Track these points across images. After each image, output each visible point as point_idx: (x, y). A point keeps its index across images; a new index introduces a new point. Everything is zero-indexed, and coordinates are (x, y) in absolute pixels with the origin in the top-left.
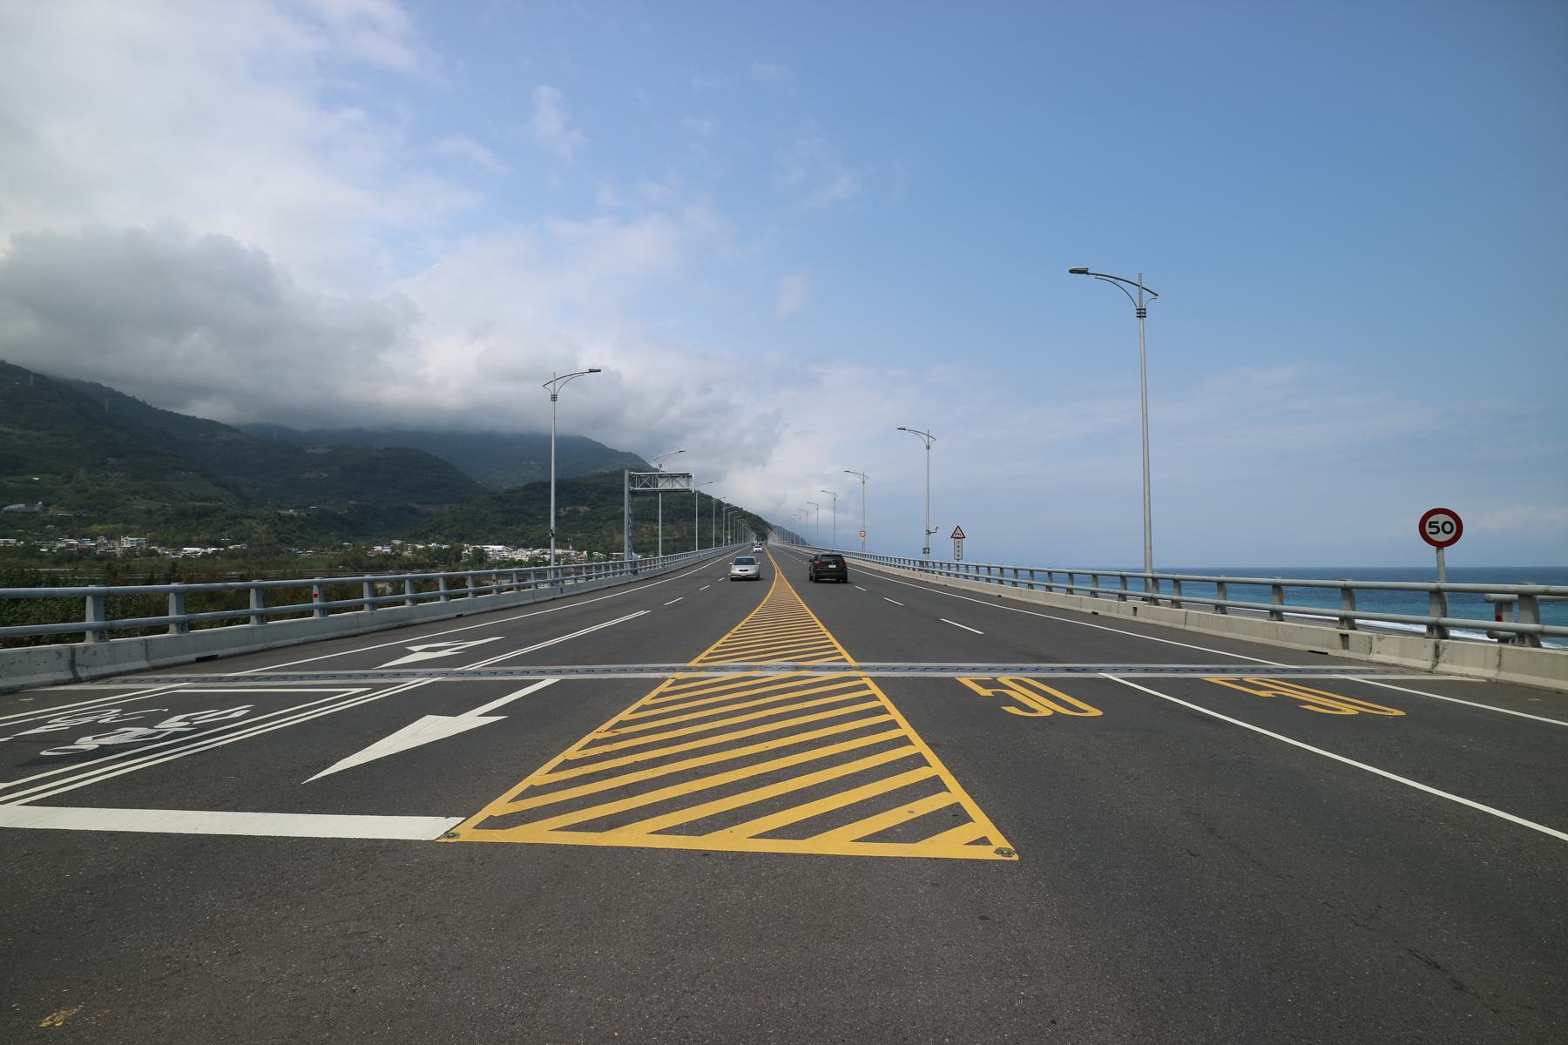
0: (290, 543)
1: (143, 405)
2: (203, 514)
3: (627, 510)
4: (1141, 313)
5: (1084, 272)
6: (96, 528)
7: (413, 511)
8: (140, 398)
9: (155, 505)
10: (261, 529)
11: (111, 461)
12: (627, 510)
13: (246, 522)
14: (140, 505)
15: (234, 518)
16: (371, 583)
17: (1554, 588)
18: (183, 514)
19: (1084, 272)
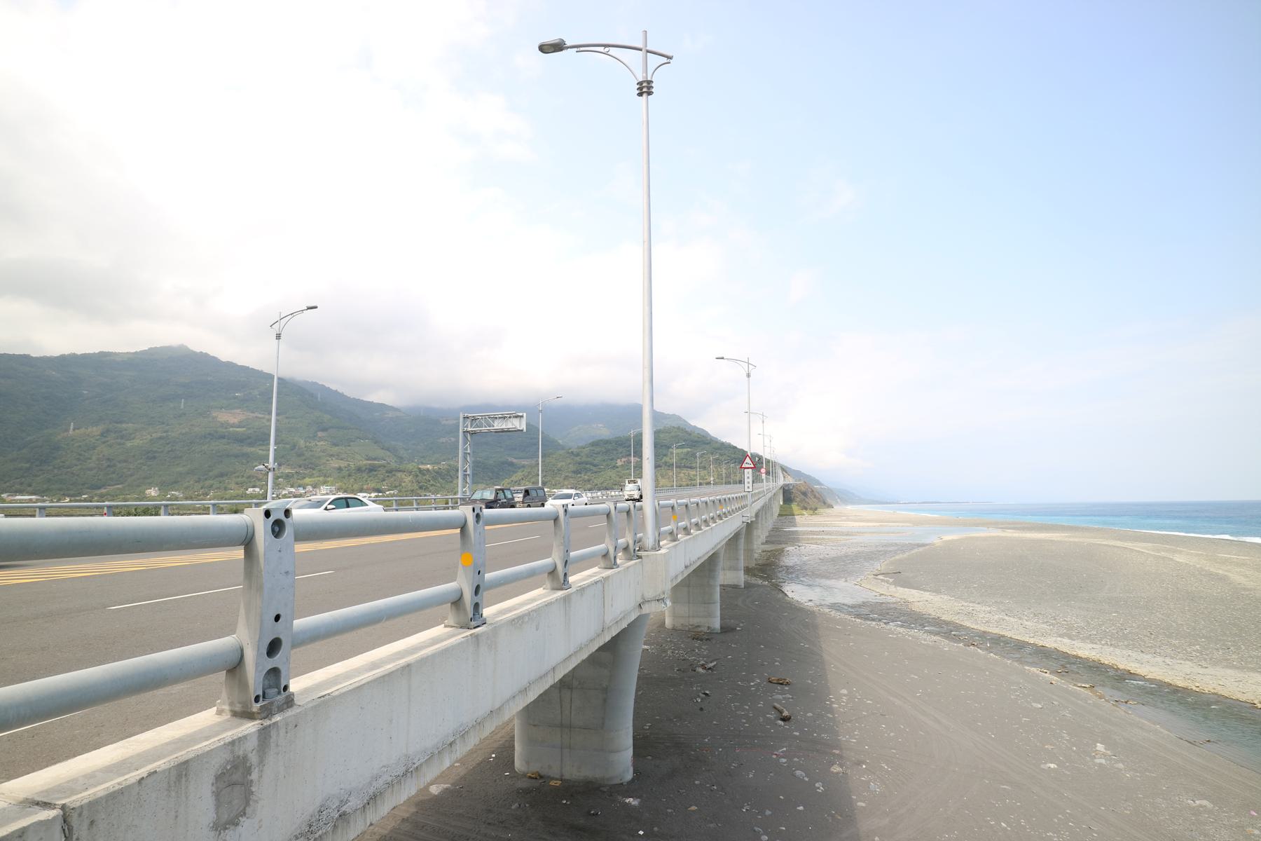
0: (426, 489)
1: (342, 395)
2: (372, 469)
3: (272, 447)
4: (645, 88)
5: (558, 47)
6: (307, 480)
7: (512, 464)
8: (340, 391)
9: (343, 464)
10: (408, 479)
11: (320, 434)
12: (272, 447)
13: (399, 474)
14: (335, 463)
15: (390, 471)
16: (166, 506)
17: (1119, 543)
18: (359, 470)
19: (558, 47)
